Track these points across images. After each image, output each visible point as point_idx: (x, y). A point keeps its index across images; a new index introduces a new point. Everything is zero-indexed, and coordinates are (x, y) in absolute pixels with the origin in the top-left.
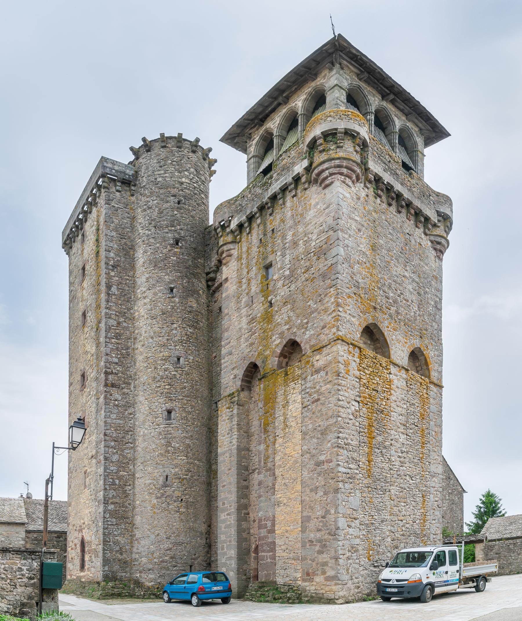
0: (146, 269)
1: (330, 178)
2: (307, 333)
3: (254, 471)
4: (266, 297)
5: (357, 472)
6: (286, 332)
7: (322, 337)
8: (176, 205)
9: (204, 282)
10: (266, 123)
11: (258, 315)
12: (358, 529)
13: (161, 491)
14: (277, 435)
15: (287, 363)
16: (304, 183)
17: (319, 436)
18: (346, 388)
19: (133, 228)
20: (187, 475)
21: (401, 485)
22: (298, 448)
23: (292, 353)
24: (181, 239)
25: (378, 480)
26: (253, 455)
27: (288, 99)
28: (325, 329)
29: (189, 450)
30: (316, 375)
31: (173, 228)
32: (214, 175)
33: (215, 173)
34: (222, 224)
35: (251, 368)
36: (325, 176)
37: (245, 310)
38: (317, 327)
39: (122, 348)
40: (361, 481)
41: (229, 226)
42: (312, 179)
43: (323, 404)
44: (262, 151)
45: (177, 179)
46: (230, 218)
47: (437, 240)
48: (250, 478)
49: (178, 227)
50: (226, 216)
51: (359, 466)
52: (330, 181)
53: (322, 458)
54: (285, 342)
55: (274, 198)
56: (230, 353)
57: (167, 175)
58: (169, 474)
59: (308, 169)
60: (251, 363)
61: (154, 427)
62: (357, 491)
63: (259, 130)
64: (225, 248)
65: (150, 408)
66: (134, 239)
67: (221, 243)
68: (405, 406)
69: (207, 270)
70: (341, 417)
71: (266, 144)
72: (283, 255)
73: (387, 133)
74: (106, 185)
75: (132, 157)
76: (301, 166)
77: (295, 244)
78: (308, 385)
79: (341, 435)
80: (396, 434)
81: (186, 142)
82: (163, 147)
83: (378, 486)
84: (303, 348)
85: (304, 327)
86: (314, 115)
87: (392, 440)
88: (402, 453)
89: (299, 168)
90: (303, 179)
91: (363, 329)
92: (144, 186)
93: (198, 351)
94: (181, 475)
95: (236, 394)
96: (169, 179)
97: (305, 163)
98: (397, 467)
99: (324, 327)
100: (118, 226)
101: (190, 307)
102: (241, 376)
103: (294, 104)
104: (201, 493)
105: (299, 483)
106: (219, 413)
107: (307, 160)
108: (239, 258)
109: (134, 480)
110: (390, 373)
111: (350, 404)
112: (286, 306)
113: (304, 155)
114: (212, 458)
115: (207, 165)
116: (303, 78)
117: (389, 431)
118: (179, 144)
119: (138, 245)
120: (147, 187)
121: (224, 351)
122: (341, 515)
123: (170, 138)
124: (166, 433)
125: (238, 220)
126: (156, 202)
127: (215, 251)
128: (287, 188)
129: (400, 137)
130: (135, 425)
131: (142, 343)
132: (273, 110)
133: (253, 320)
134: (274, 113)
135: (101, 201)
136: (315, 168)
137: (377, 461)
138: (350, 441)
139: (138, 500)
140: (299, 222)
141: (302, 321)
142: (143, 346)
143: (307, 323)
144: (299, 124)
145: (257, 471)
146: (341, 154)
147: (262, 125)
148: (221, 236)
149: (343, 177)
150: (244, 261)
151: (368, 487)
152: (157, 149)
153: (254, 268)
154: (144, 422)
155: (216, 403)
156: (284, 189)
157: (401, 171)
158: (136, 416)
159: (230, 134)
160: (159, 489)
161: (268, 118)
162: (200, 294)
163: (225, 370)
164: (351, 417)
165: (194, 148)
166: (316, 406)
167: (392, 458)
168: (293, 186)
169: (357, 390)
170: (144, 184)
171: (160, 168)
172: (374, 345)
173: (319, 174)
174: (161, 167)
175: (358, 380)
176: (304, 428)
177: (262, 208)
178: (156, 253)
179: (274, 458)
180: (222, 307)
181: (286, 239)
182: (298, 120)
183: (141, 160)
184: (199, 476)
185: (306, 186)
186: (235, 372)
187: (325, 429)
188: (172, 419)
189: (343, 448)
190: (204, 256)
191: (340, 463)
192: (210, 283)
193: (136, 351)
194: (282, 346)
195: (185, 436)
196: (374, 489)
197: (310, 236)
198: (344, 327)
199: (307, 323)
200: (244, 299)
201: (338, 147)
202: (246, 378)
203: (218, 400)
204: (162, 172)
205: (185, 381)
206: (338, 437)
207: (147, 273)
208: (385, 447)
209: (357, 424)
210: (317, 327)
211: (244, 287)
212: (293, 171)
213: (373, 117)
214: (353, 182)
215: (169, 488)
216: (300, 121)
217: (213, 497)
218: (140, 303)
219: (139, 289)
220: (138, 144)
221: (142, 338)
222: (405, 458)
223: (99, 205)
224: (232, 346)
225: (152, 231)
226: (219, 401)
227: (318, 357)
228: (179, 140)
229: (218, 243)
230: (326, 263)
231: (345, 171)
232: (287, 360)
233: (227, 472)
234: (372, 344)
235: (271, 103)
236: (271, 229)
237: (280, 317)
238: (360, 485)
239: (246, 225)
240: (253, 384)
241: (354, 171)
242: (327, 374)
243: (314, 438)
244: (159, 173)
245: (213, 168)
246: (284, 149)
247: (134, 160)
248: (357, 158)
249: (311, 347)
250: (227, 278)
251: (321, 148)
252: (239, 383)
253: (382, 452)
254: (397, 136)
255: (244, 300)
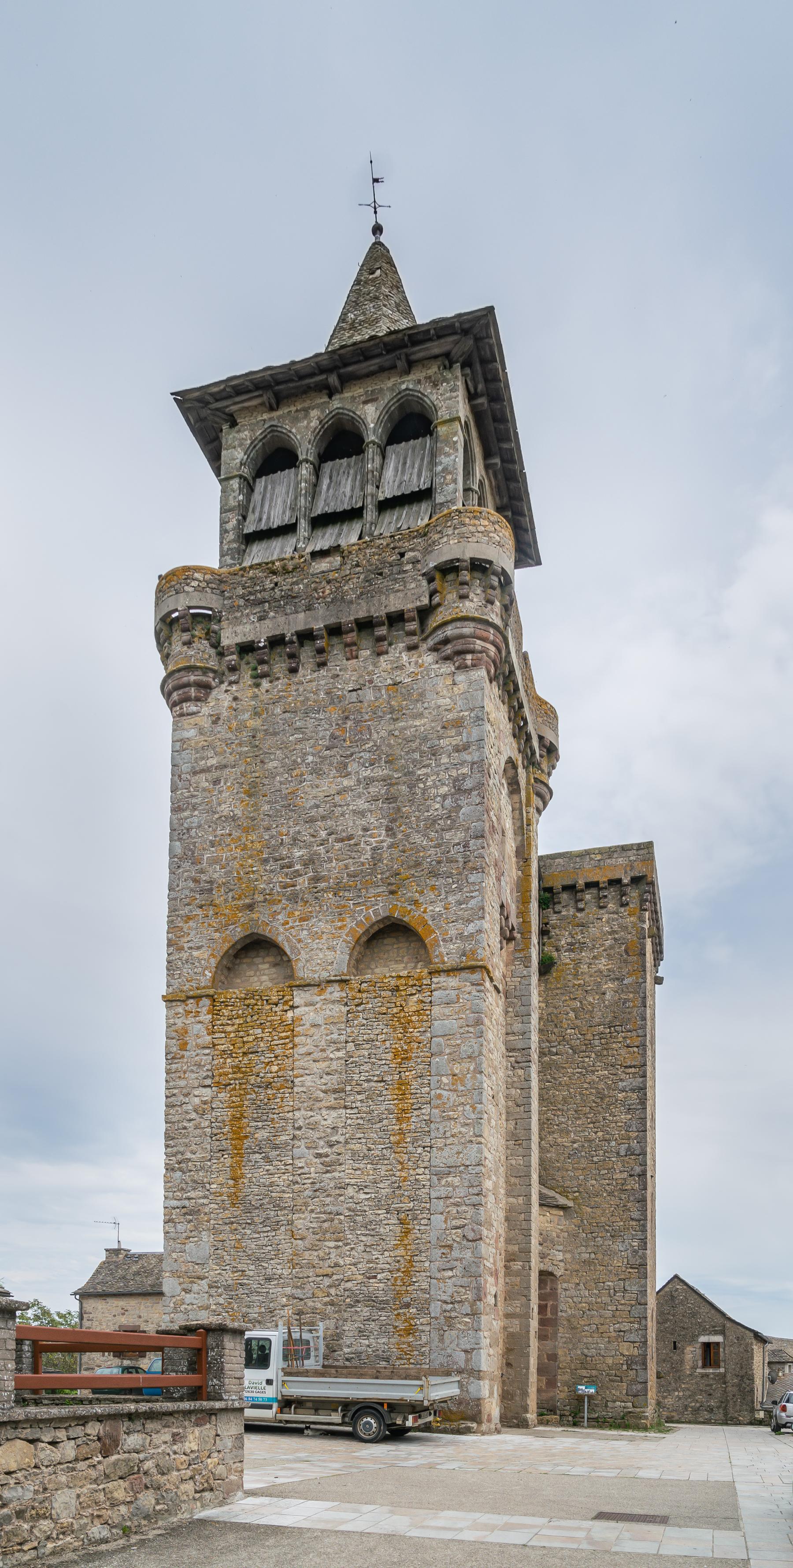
0: (361, 757)
12: (206, 1295)
21: (328, 1209)
47: (437, 640)
62: (204, 1233)
88: (331, 1146)
122: (167, 1274)
138: (189, 1155)
151: (232, 1223)
164: (193, 1115)
238: (212, 1222)
241: (188, 685)
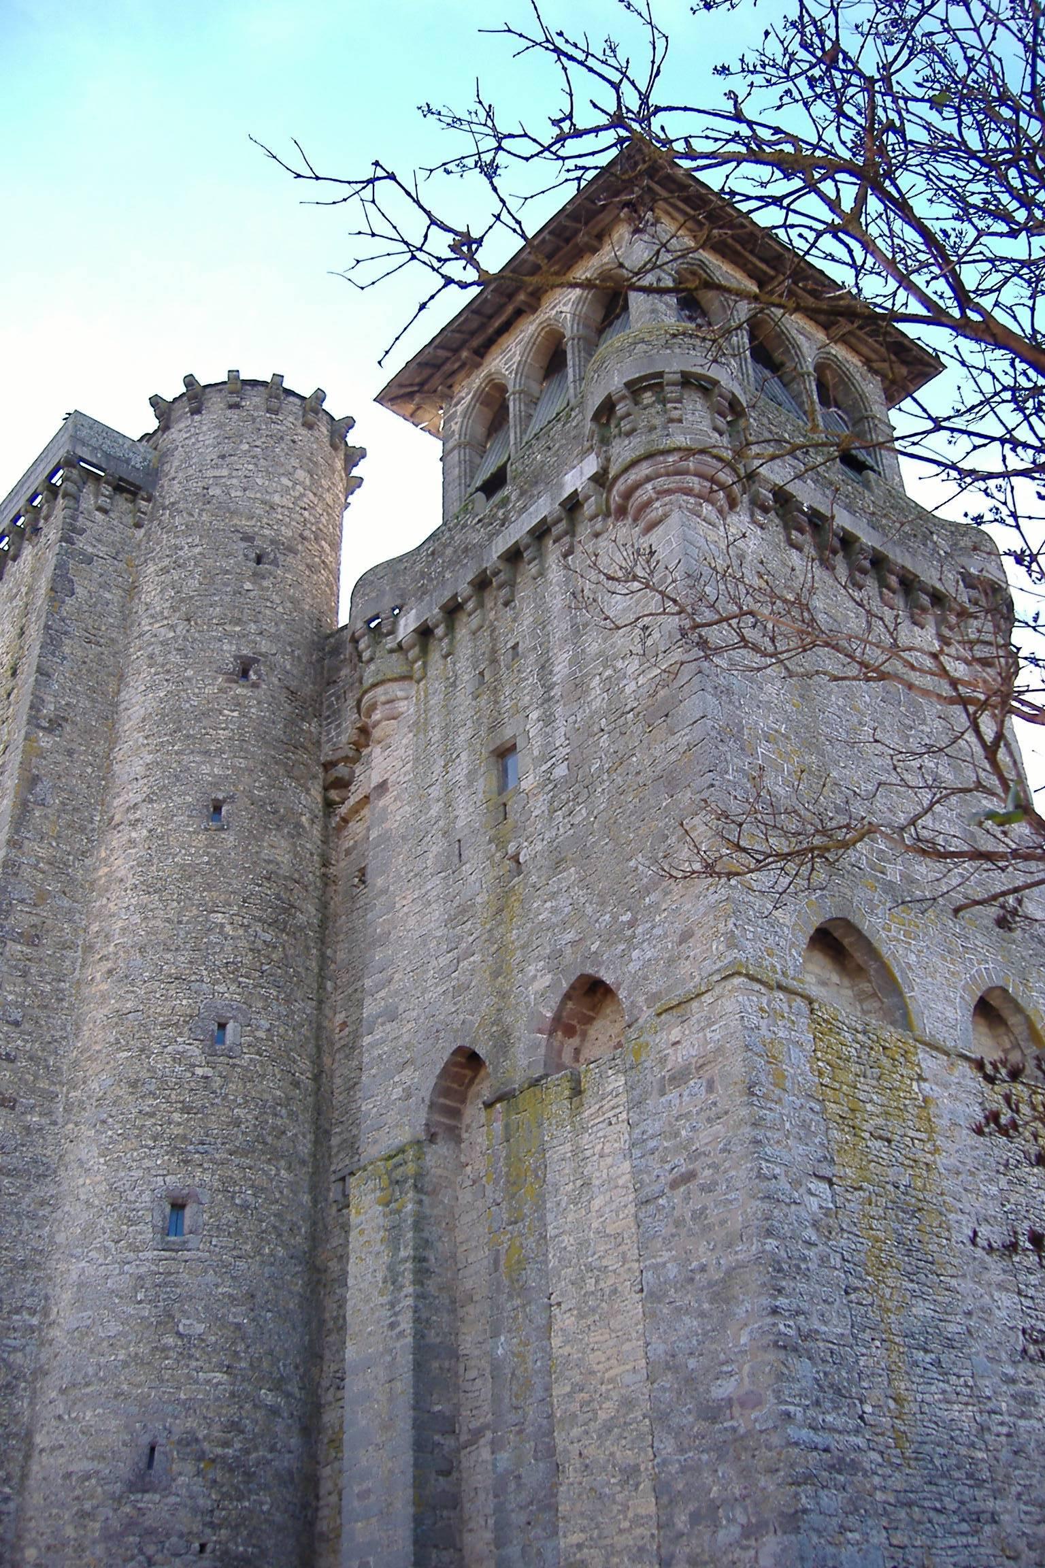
0: (146, 737)
1: (657, 504)
2: (635, 954)
3: (477, 1434)
4: (499, 841)
5: (859, 1441)
6: (569, 950)
7: (685, 967)
9: (316, 792)
10: (488, 358)
11: (479, 899)
15: (577, 1051)
16: (593, 518)
17: (706, 1306)
18: (777, 1135)
19: (126, 619)
20: (226, 1444)
22: (634, 1345)
23: (589, 1020)
24: (258, 661)
25: (943, 1476)
26: (472, 1374)
27: (539, 299)
29: (241, 1347)
30: (675, 1093)
31: (238, 629)
32: (358, 491)
34: (373, 625)
35: (455, 1064)
36: (645, 498)
37: (436, 880)
38: (666, 935)
40: (877, 1480)
41: (392, 632)
42: (613, 507)
43: (708, 1189)
44: (481, 431)
45: (258, 495)
46: (397, 611)
48: (465, 1464)
49: (253, 627)
50: (388, 602)
51: (861, 1418)
52: (660, 512)
53: (724, 1389)
54: (565, 985)
55: (514, 556)
56: (392, 1015)
57: (234, 481)
59: (601, 480)
60: (460, 1050)
61: (119, 1257)
64: (380, 694)
67: (368, 681)
69: (327, 754)
70: (777, 1237)
71: (488, 414)
72: (548, 720)
73: (786, 379)
74: (71, 487)
75: (152, 424)
76: (582, 473)
77: (579, 686)
78: (653, 1127)
81: (291, 399)
83: (947, 1500)
84: (626, 1004)
86: (602, 340)
87: (969, 1314)
89: (576, 479)
90: (589, 508)
91: (811, 938)
92: (173, 504)
93: (288, 1001)
94: (206, 1446)
95: (410, 1154)
96: (239, 494)
97: (591, 465)
98: (1007, 1418)
100: (86, 608)
101: (269, 862)
102: (426, 1092)
103: (554, 312)
105: (646, 1485)
106: (352, 1217)
107: (593, 456)
108: (420, 727)
109: (28, 1457)
110: (921, 1078)
111: (802, 1190)
112: (565, 870)
113: (587, 444)
115: (339, 464)
117: (954, 1282)
119: (135, 666)
120: (181, 506)
121: (370, 1008)
123: (254, 383)
124: (159, 1279)
125: (418, 617)
126: (199, 549)
127: (351, 703)
128: (548, 530)
129: (821, 386)
130: (52, 1242)
131: (110, 965)
132: (506, 327)
133: (464, 911)
134: (506, 335)
135: (51, 532)
136: (616, 478)
137: (927, 1397)
138: (816, 1325)
140: (586, 625)
141: (615, 918)
142: (110, 972)
143: (632, 924)
144: (570, 363)
145: (489, 1435)
146: (680, 440)
147: (478, 366)
148: (371, 660)
149: (692, 500)
150: (435, 735)
152: (216, 406)
153: (464, 756)
154: (89, 1229)
155: (343, 1179)
156: (541, 532)
157: (837, 472)
159: (401, 386)
160: (118, 1500)
162: (302, 826)
163: (374, 1071)
164: (810, 1234)
165: (311, 417)
166: (687, 1198)
167: (980, 1382)
168: (562, 526)
170: (172, 500)
171: (220, 461)
172: (852, 987)
173: (628, 495)
174: (223, 457)
175: (817, 1108)
176: (648, 1275)
179: (548, 1389)
180: (369, 870)
181: (551, 673)
182: (565, 352)
184: (272, 1449)
185: (599, 526)
186: (409, 1076)
187: (723, 1280)
188: (186, 1229)
189: (795, 1350)
190: (318, 715)
191: (791, 1408)
192: (334, 795)
193: (86, 991)
194: (558, 999)
195: (230, 1296)
196: (932, 1514)
197: (619, 664)
198: (750, 936)
199: (632, 924)
200: (436, 848)
201: (671, 421)
202: (442, 1100)
203: (346, 1171)
204: (225, 472)
205: (240, 1100)
206: (775, 1311)
207: (150, 753)
208: (950, 1344)
209: (836, 1260)
210: (666, 935)
211: (435, 810)
212: (561, 486)
213: (746, 340)
214: (720, 511)
216: (569, 356)
218: (116, 840)
219: (118, 795)
220: (172, 389)
221: (111, 949)
222: (1030, 1383)
223: (43, 540)
224: (397, 992)
225: (179, 629)
226: (352, 1174)
227: (675, 1034)
228: (275, 390)
229: (361, 681)
230: (672, 741)
231: (694, 483)
232: (575, 1041)
233: (378, 1440)
234: (846, 982)
235: (500, 308)
237: (548, 904)
239: (440, 631)
240: (467, 1119)
242: (710, 1087)
243: (687, 1312)
244: (217, 473)
245: (355, 472)
246: (534, 427)
247: (156, 431)
248: (723, 444)
249: (653, 998)
250: (385, 782)
252: (422, 1116)
253: (938, 1363)
254: (814, 384)
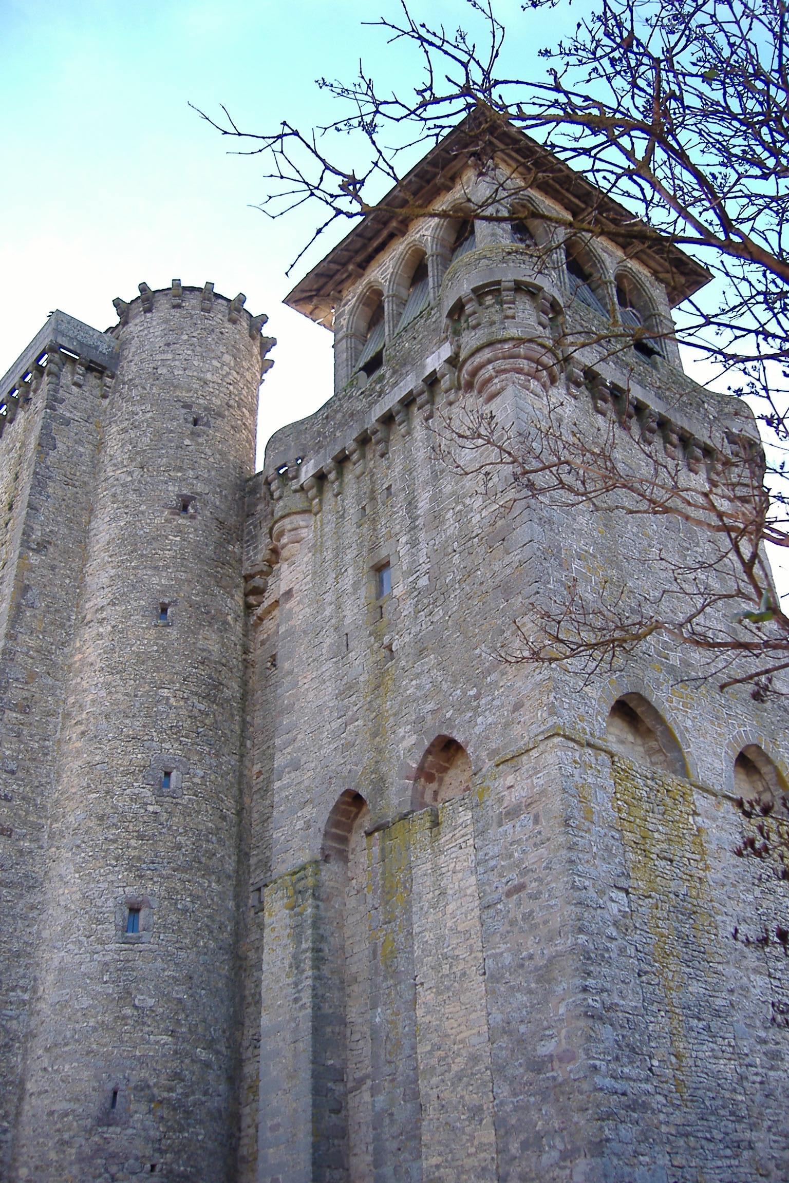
0: (111, 556)
1: (496, 381)
2: (479, 720)
3: (361, 1082)
4: (377, 635)
5: (649, 1087)
6: (429, 717)
7: (517, 730)
8: (191, 426)
9: (239, 598)
10: (369, 270)
11: (361, 679)
13: (96, 1139)
14: (418, 980)
15: (436, 793)
17: (533, 985)
18: (587, 857)
19: (95, 467)
20: (171, 1089)
23: (445, 770)
24: (194, 499)
25: (712, 1113)
27: (407, 226)
28: (522, 710)
30: (510, 824)
31: (179, 474)
32: (270, 370)
33: (274, 344)
34: (281, 472)
35: (344, 803)
36: (487, 375)
37: (330, 664)
38: (502, 706)
39: (31, 736)
40: (662, 1117)
41: (296, 477)
43: (534, 897)
44: (363, 325)
45: (195, 374)
46: (299, 461)
48: (351, 1104)
49: (191, 473)
50: (293, 454)
51: (650, 1070)
52: (498, 386)
53: (547, 1048)
54: (427, 744)
55: (388, 420)
56: (296, 766)
57: (177, 363)
58: (122, 1087)
59: (453, 362)
60: (347, 793)
63: (357, 285)
64: (287, 523)
65: (84, 894)
66: (96, 488)
67: (278, 514)
68: (750, 898)
69: (247, 569)
70: (587, 933)
71: (369, 312)
72: (414, 543)
75: (115, 320)
77: (437, 518)
78: (493, 850)
79: (590, 982)
80: (741, 974)
81: (220, 301)
82: (174, 307)
83: (715, 1132)
84: (473, 757)
85: (468, 705)
87: (732, 991)
89: (435, 361)
90: (445, 383)
92: (131, 380)
93: (217, 755)
94: (155, 1091)
95: (310, 870)
96: (180, 372)
97: (446, 351)
98: (760, 1070)
99: (518, 707)
100: (65, 459)
101: (203, 650)
102: (322, 824)
103: (418, 236)
104: (210, 1145)
108: (317, 548)
109: (21, 1099)
110: (695, 813)
111: (606, 898)
113: (443, 335)
114: (245, 1043)
115: (256, 350)
116: (431, 185)
117: (720, 967)
118: (207, 304)
119: (102, 502)
120: (137, 381)
121: (280, 761)
123: (192, 289)
125: (315, 466)
126: (149, 415)
127: (265, 530)
128: (414, 400)
129: (620, 291)
131: (83, 728)
133: (351, 687)
134: (382, 253)
135: (39, 402)
136: (465, 361)
137: (700, 1054)
138: (617, 1000)
139: (26, 1164)
140: (442, 472)
141: (464, 693)
142: (83, 733)
143: (477, 697)
144: (430, 274)
145: (369, 1082)
147: (361, 276)
148: (280, 498)
149: (522, 377)
150: (329, 555)
152: (163, 306)
153: (350, 571)
154: (67, 928)
155: (259, 890)
156: (408, 402)
157: (632, 356)
158: (44, 916)
160: (89, 1131)
161: (373, 263)
162: (228, 624)
163: (282, 808)
164: (612, 931)
165: (235, 315)
166: (519, 904)
167: (740, 1043)
168: (425, 397)
169: (617, 860)
170: (130, 377)
171: (166, 348)
172: (643, 745)
173: (474, 373)
174: (168, 345)
175: (617, 836)
176: (489, 962)
177: (364, 441)
178: (138, 524)
179: (414, 1048)
180: (278, 657)
181: (416, 507)
182: (426, 266)
183: (131, 327)
186: (308, 812)
187: (546, 966)
189: (600, 1018)
190: (240, 539)
191: (598, 1063)
192: (252, 600)
193: (65, 748)
194: (421, 754)
195: (174, 977)
196: (704, 1142)
197: (468, 501)
198: (566, 706)
199: (477, 697)
200: (329, 640)
201: (507, 317)
202: (334, 830)
203: (262, 884)
204: (170, 356)
205: (181, 830)
206: (585, 989)
207: (113, 568)
208: (717, 1014)
209: (631, 951)
210: (502, 706)
212: (424, 367)
214: (544, 386)
215: (118, 1130)
216: (430, 269)
217: (243, 1159)
218: (88, 633)
219: (89, 600)
220: (130, 294)
221: (84, 716)
222: (777, 1043)
223: (32, 407)
224: (299, 748)
225: (135, 475)
227: (510, 780)
228: (208, 294)
229: (272, 513)
230: (507, 559)
231: (524, 364)
232: (434, 786)
234: (639, 741)
235: (377, 233)
236: (385, 487)
237: (414, 682)
239: (332, 476)
240: (352, 844)
242: (536, 820)
243: (519, 990)
244: (164, 357)
245: (268, 356)
246: (404, 322)
247: (117, 325)
248: (546, 335)
249: (493, 753)
250: (291, 590)
251: (472, 321)
252: (319, 842)
253: (708, 1028)
254: (614, 290)
255: (328, 641)
